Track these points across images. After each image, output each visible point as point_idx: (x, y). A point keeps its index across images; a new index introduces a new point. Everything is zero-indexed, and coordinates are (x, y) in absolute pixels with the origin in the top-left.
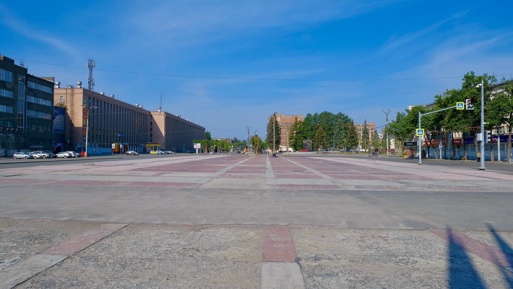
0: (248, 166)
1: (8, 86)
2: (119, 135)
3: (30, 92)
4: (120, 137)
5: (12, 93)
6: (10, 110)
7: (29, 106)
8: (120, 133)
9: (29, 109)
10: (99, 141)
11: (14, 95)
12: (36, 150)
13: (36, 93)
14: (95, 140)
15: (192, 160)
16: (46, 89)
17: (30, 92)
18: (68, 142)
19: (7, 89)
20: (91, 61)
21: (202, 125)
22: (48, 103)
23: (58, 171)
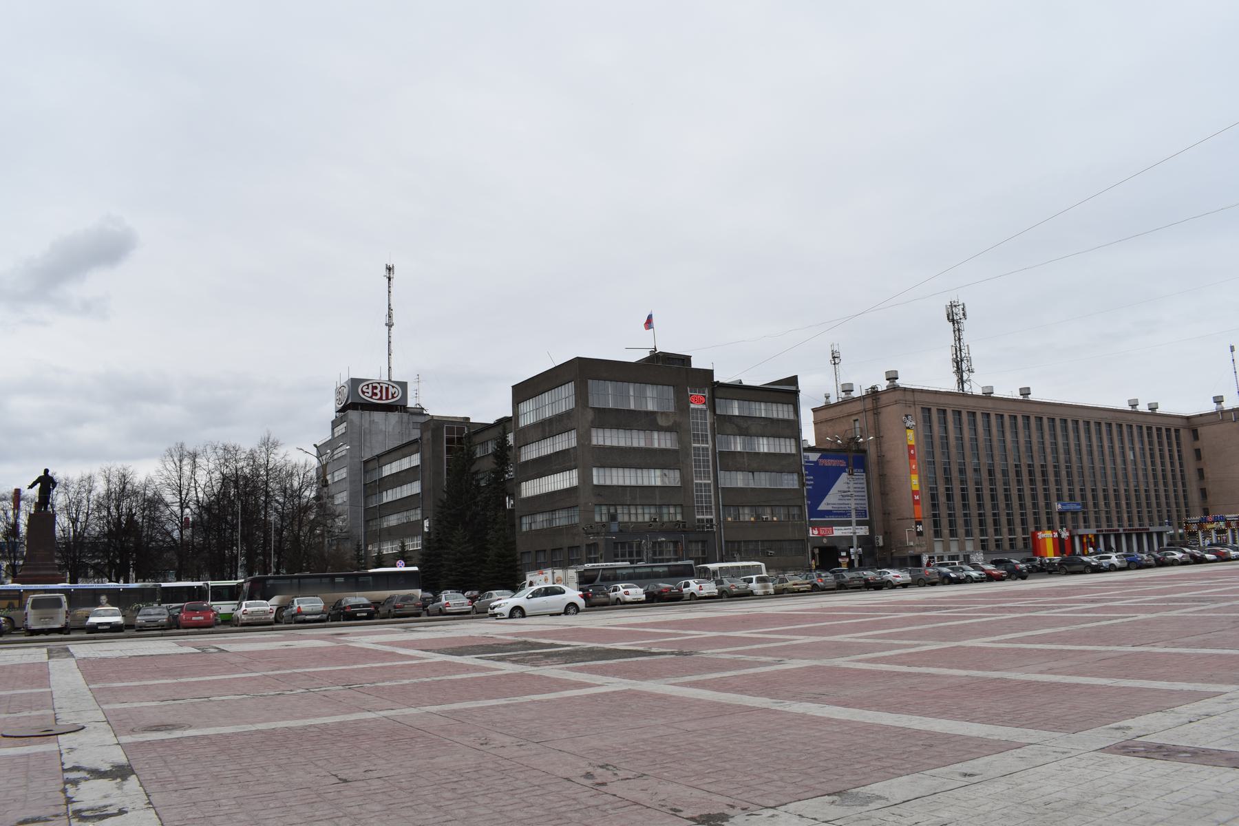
0: (904, 669)
1: (662, 421)
2: (1058, 506)
3: (724, 424)
4: (1061, 513)
5: (674, 435)
6: (673, 478)
7: (728, 461)
8: (1059, 498)
9: (726, 468)
10: (976, 531)
11: (680, 441)
12: (302, 588)
13: (745, 427)
14: (961, 531)
15: (825, 605)
16: (780, 412)
17: (724, 424)
18: (881, 544)
19: (660, 429)
20: (108, 250)
21: (459, 413)
22: (787, 447)
23: (993, 610)
